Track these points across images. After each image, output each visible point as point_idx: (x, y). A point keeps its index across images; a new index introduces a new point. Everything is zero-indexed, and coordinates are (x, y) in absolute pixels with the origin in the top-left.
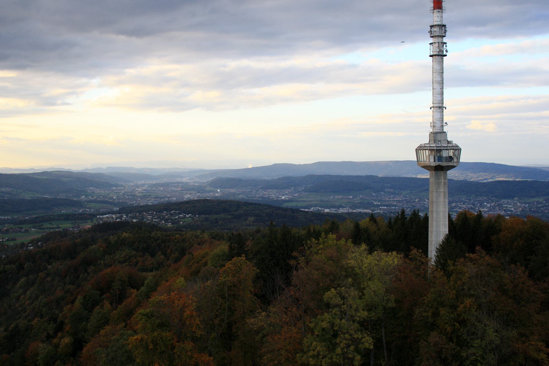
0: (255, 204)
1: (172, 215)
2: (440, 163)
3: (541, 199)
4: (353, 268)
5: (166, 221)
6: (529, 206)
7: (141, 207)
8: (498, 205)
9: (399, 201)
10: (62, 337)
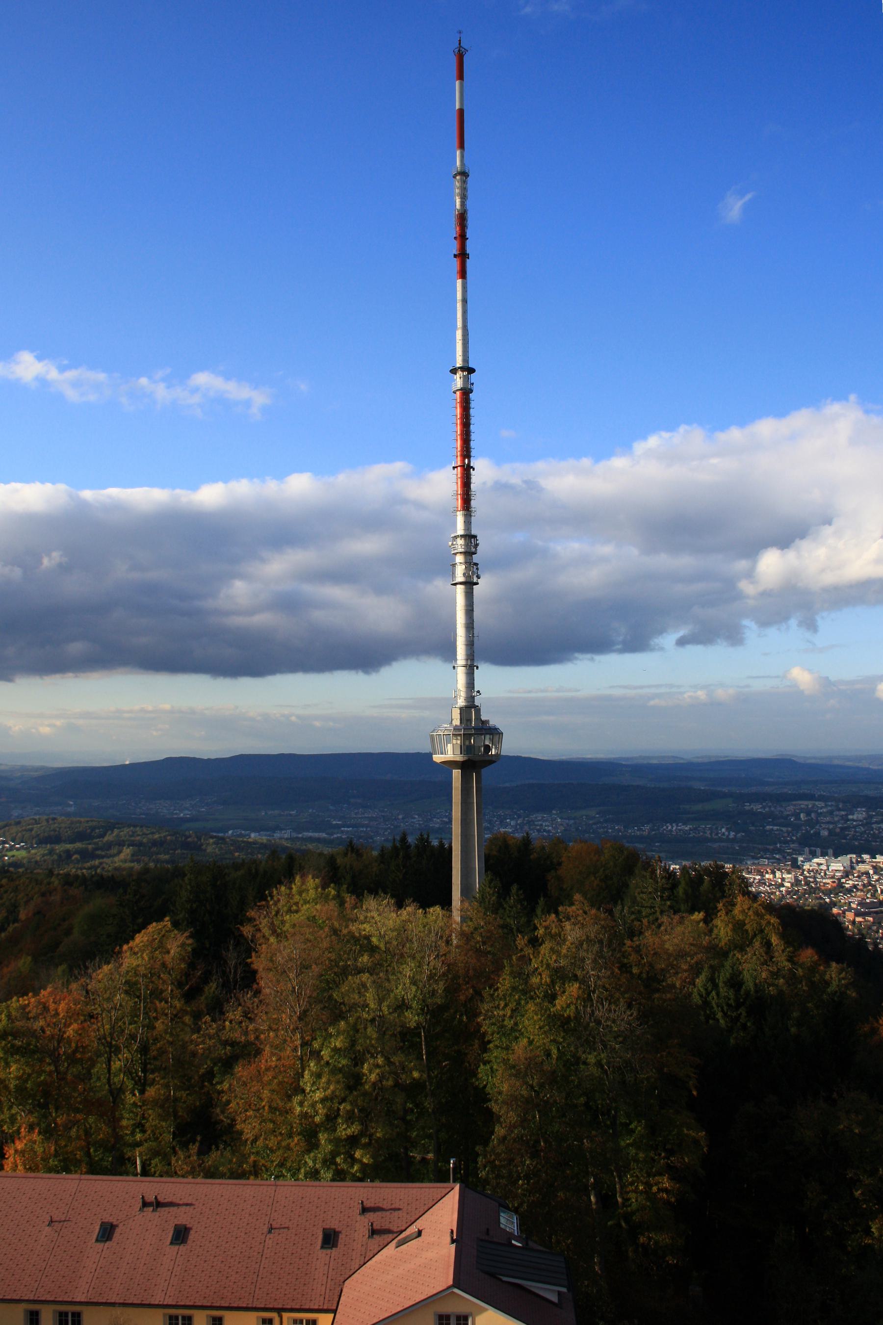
3: (592, 812)
4: (368, 938)
6: (575, 823)
8: (529, 822)
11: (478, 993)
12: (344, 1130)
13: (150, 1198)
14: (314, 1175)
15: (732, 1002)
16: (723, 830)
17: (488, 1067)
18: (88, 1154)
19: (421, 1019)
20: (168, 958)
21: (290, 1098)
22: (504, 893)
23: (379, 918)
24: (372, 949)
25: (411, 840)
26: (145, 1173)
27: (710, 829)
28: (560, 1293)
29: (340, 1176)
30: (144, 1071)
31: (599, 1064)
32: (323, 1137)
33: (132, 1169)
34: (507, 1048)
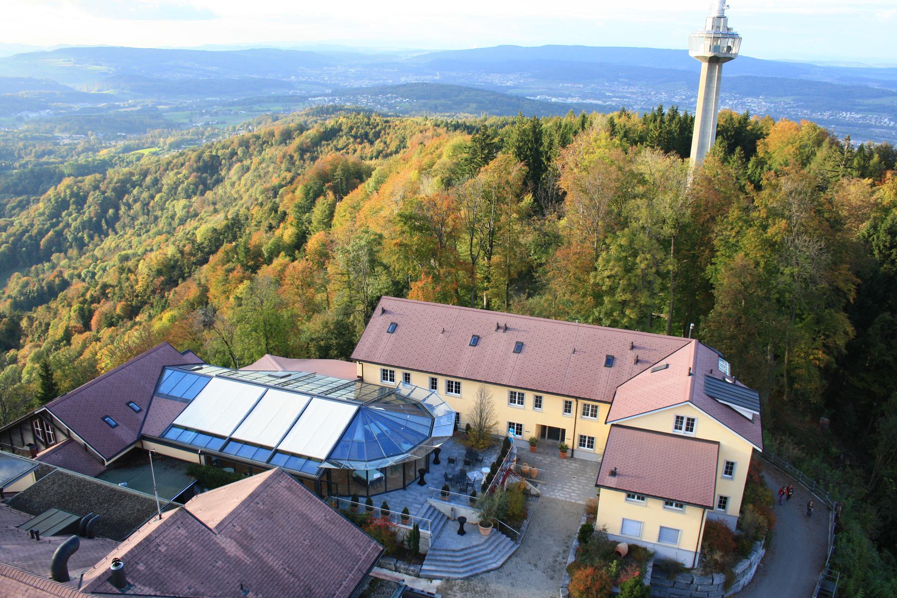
0: (478, 90)
1: (388, 99)
3: (788, 99)
5: (382, 105)
7: (355, 89)
8: (742, 103)
9: (633, 93)
10: (285, 228)
11: (713, 219)
12: (620, 296)
13: (502, 324)
14: (598, 321)
15: (887, 244)
17: (713, 267)
18: (457, 292)
19: (673, 231)
20: (510, 178)
21: (588, 273)
22: (730, 150)
23: (652, 162)
24: (643, 182)
25: (666, 111)
26: (488, 307)
27: (876, 118)
28: (754, 415)
29: (614, 324)
30: (491, 246)
31: (792, 275)
32: (606, 299)
33: (481, 303)
34: (729, 257)
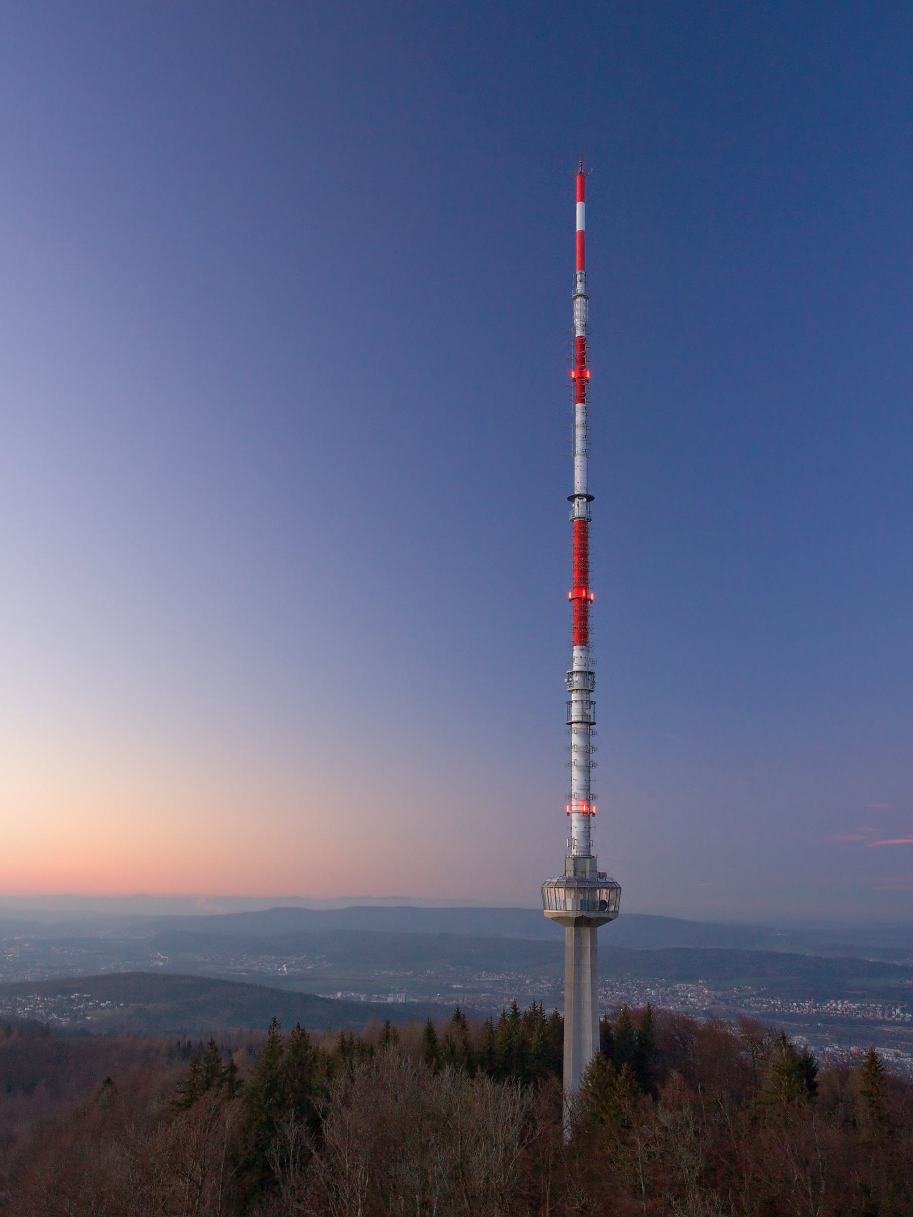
2: (586, 914)
16: (898, 1011)
